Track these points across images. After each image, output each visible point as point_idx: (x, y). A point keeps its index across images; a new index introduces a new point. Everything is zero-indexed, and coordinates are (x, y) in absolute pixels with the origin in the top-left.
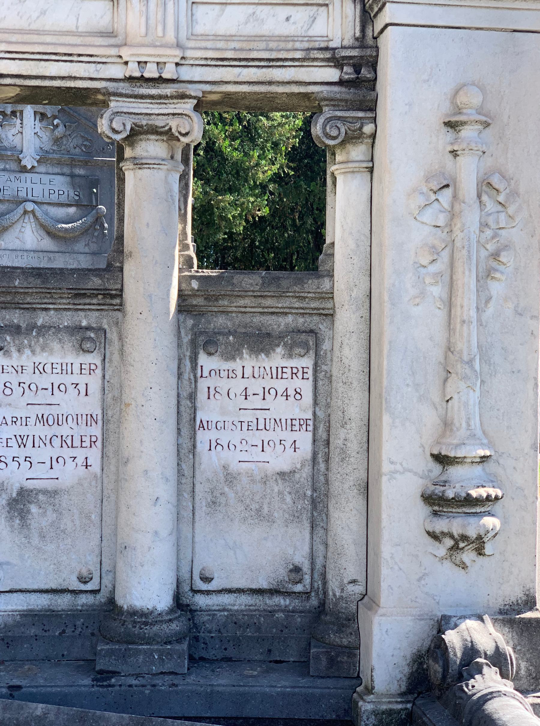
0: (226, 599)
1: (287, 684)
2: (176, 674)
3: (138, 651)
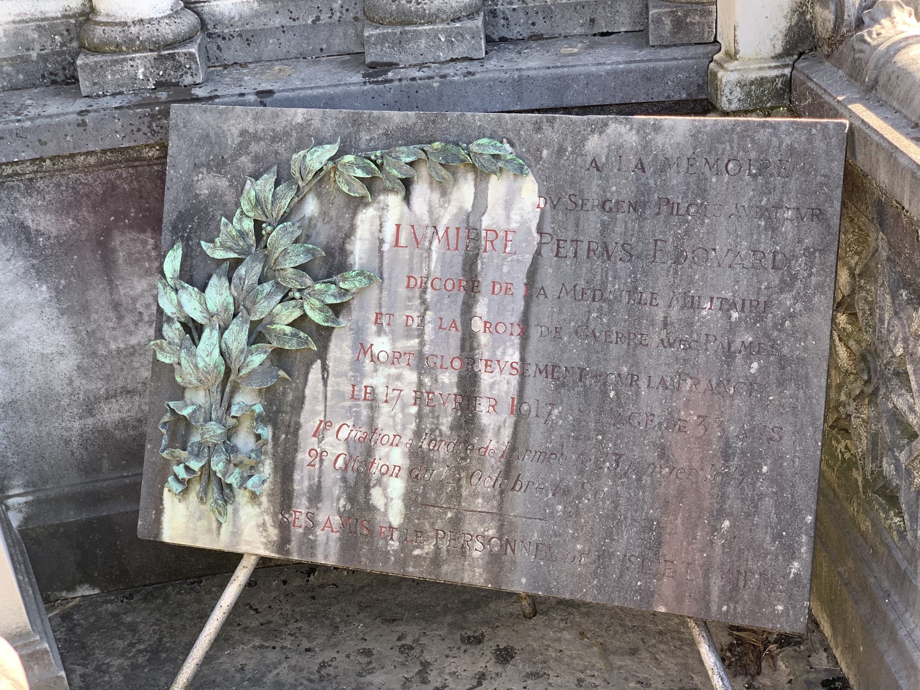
1: (620, 59)
2: (472, 59)
3: (418, 35)
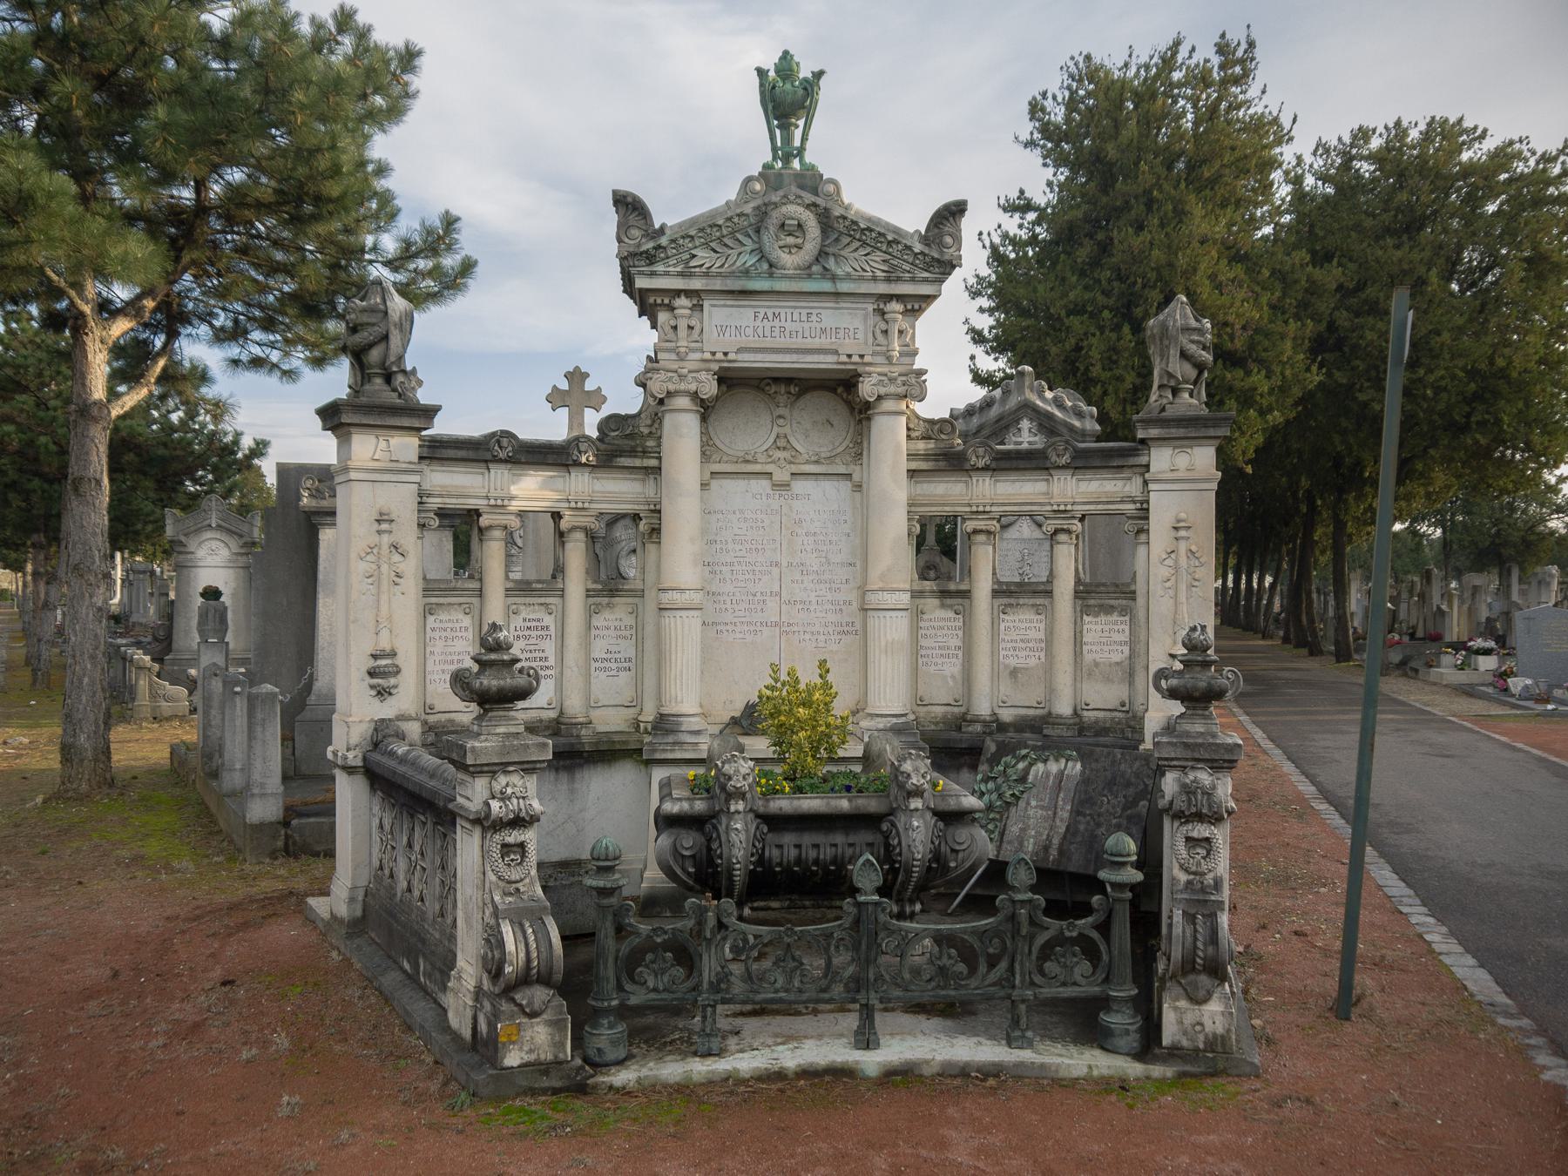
0: (1096, 713)
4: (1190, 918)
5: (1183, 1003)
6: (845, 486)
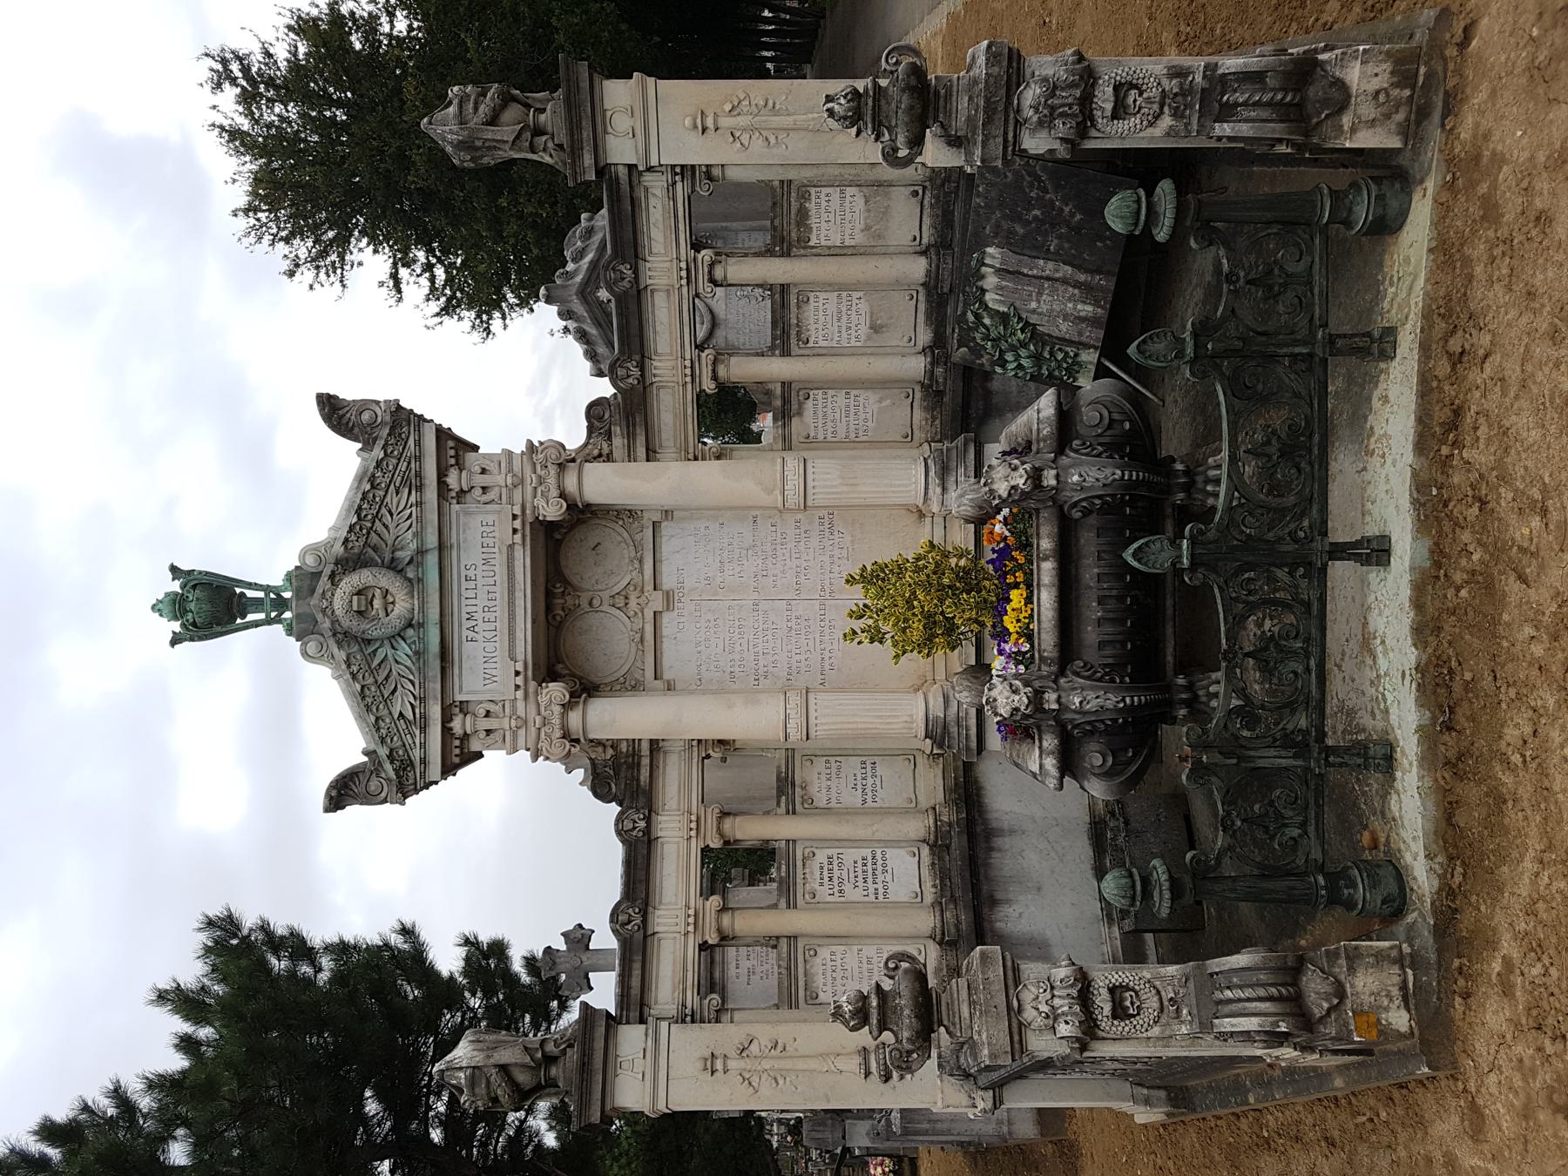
4: (1227, 112)
5: (1346, 120)
6: (667, 529)
